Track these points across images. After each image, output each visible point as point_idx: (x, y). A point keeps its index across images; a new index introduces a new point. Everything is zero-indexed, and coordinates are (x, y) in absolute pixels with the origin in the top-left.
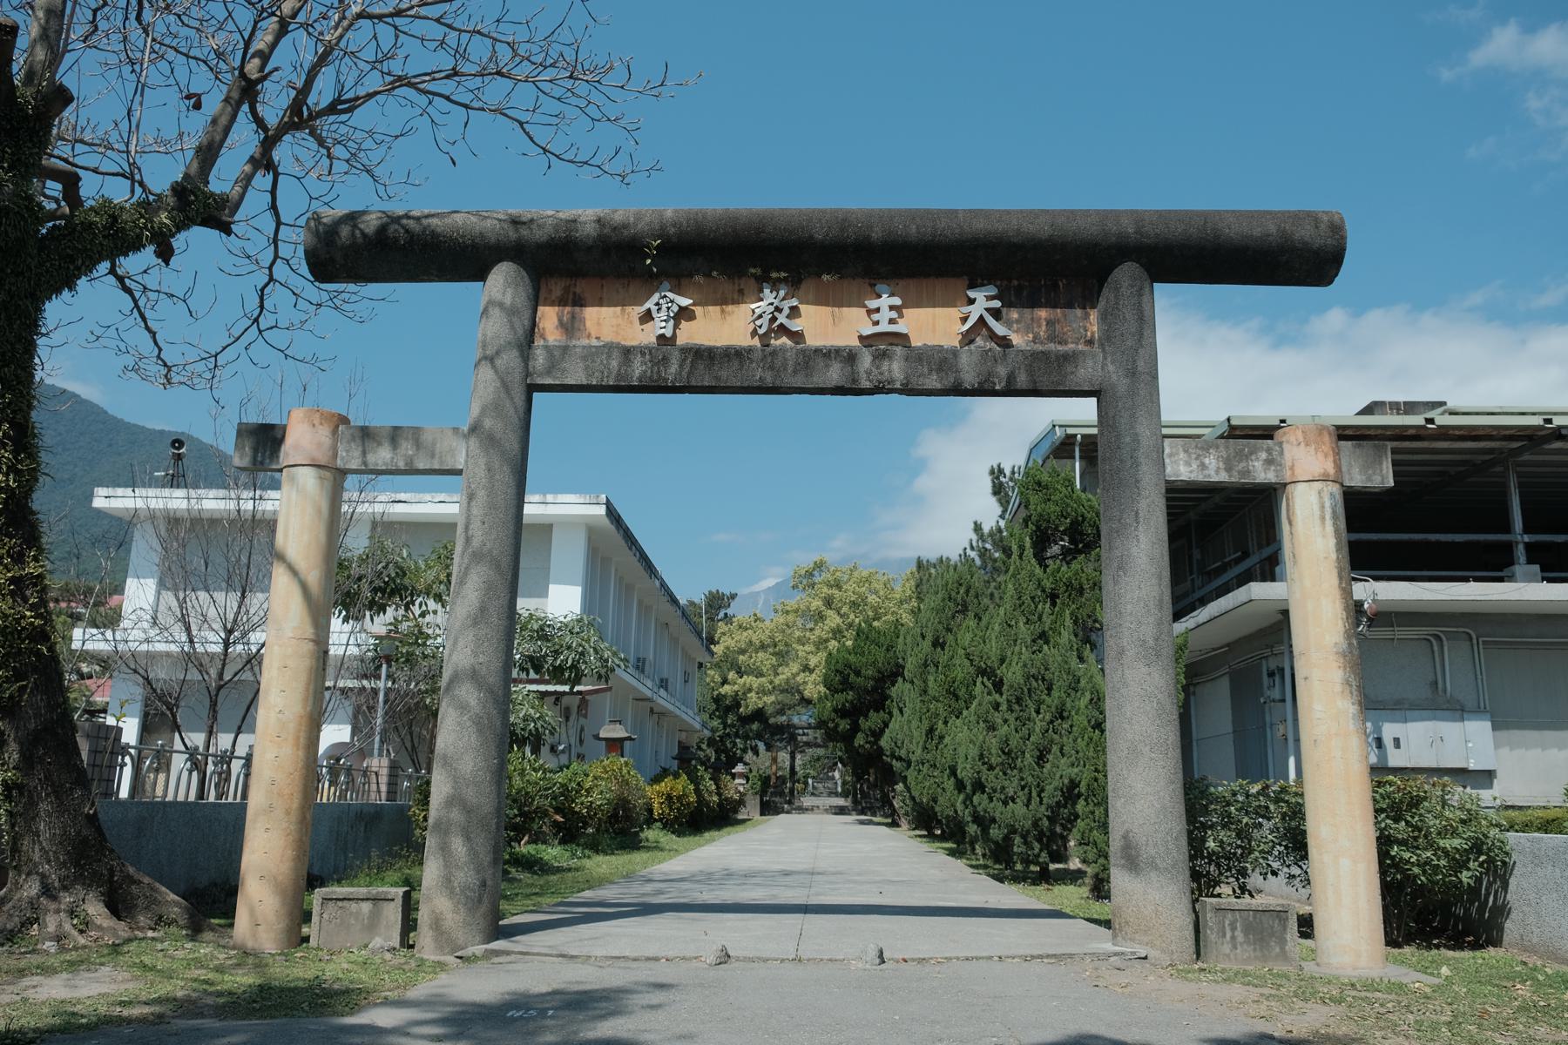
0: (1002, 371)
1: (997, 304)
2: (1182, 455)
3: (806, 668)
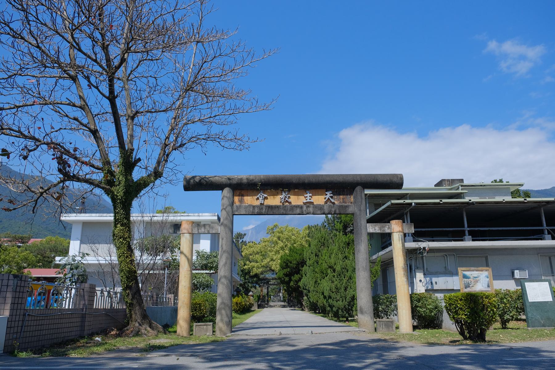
0: (333, 210)
1: (332, 195)
3: (272, 260)
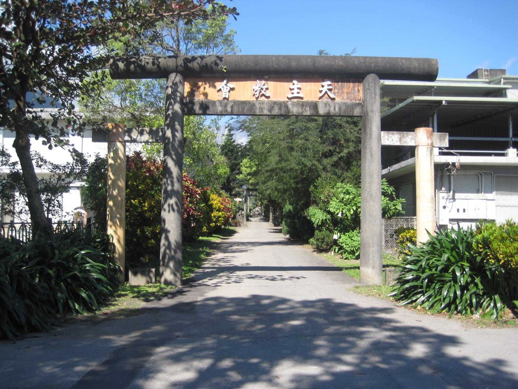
1: (330, 87)
2: (387, 137)
